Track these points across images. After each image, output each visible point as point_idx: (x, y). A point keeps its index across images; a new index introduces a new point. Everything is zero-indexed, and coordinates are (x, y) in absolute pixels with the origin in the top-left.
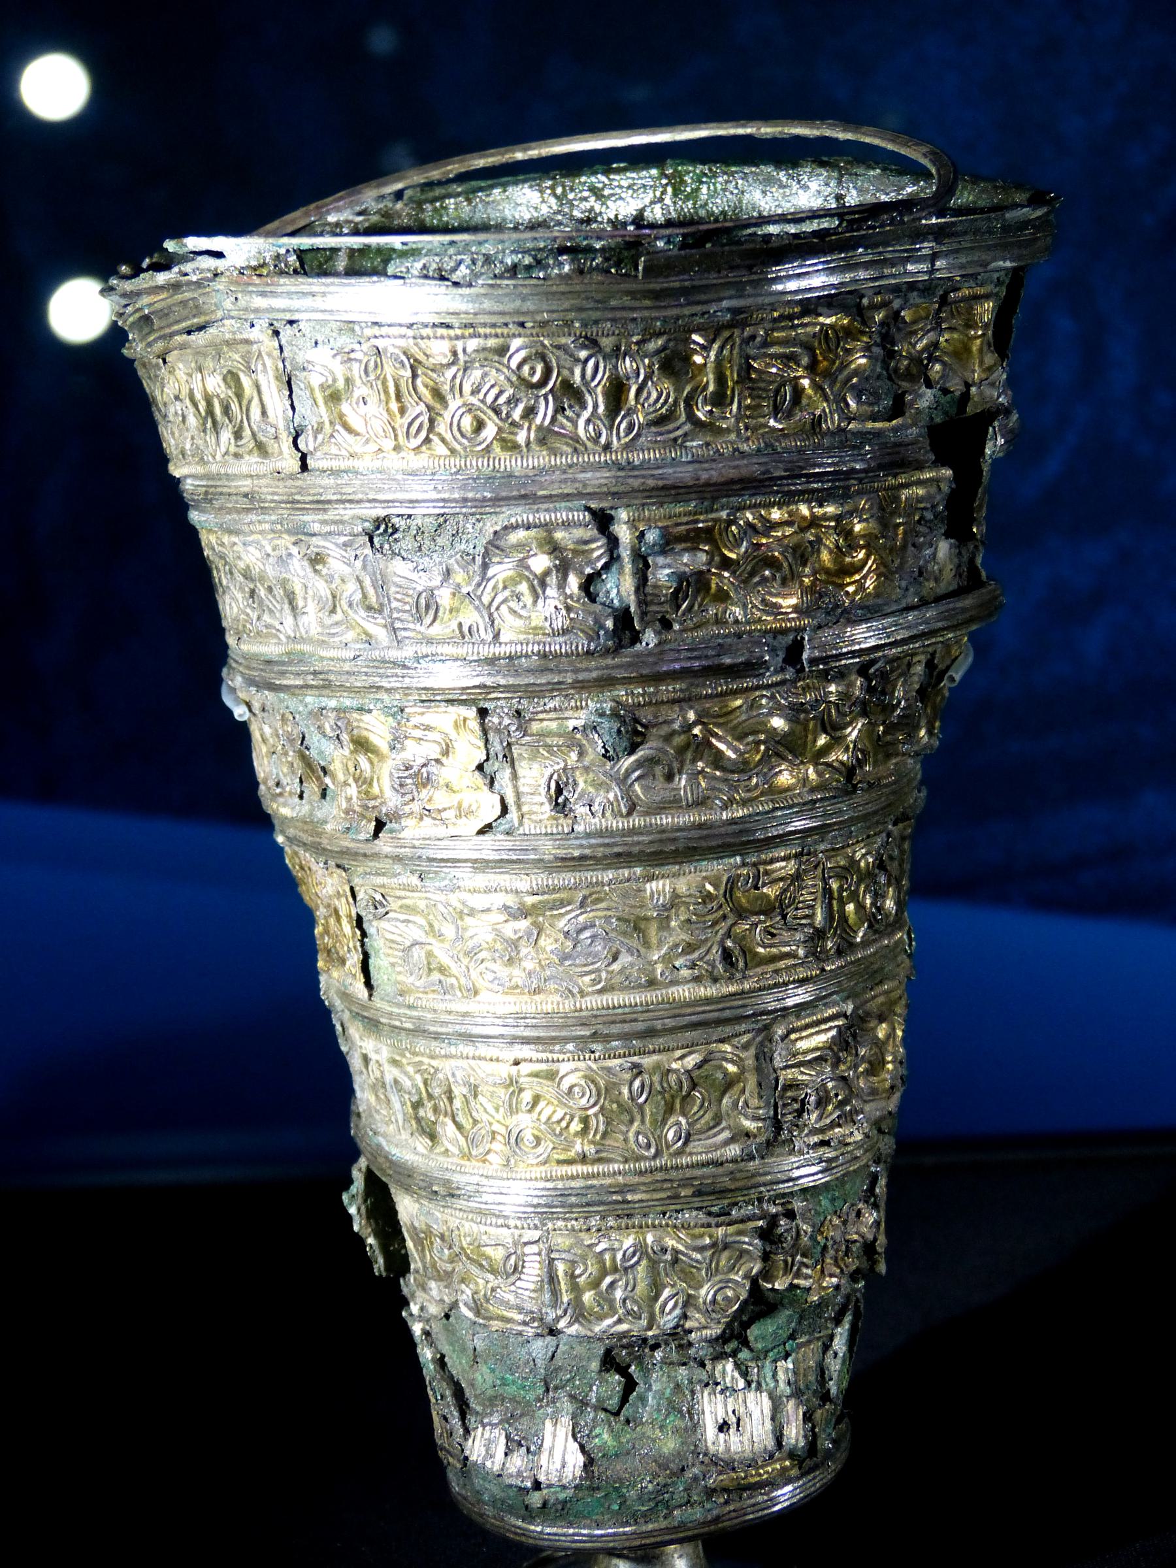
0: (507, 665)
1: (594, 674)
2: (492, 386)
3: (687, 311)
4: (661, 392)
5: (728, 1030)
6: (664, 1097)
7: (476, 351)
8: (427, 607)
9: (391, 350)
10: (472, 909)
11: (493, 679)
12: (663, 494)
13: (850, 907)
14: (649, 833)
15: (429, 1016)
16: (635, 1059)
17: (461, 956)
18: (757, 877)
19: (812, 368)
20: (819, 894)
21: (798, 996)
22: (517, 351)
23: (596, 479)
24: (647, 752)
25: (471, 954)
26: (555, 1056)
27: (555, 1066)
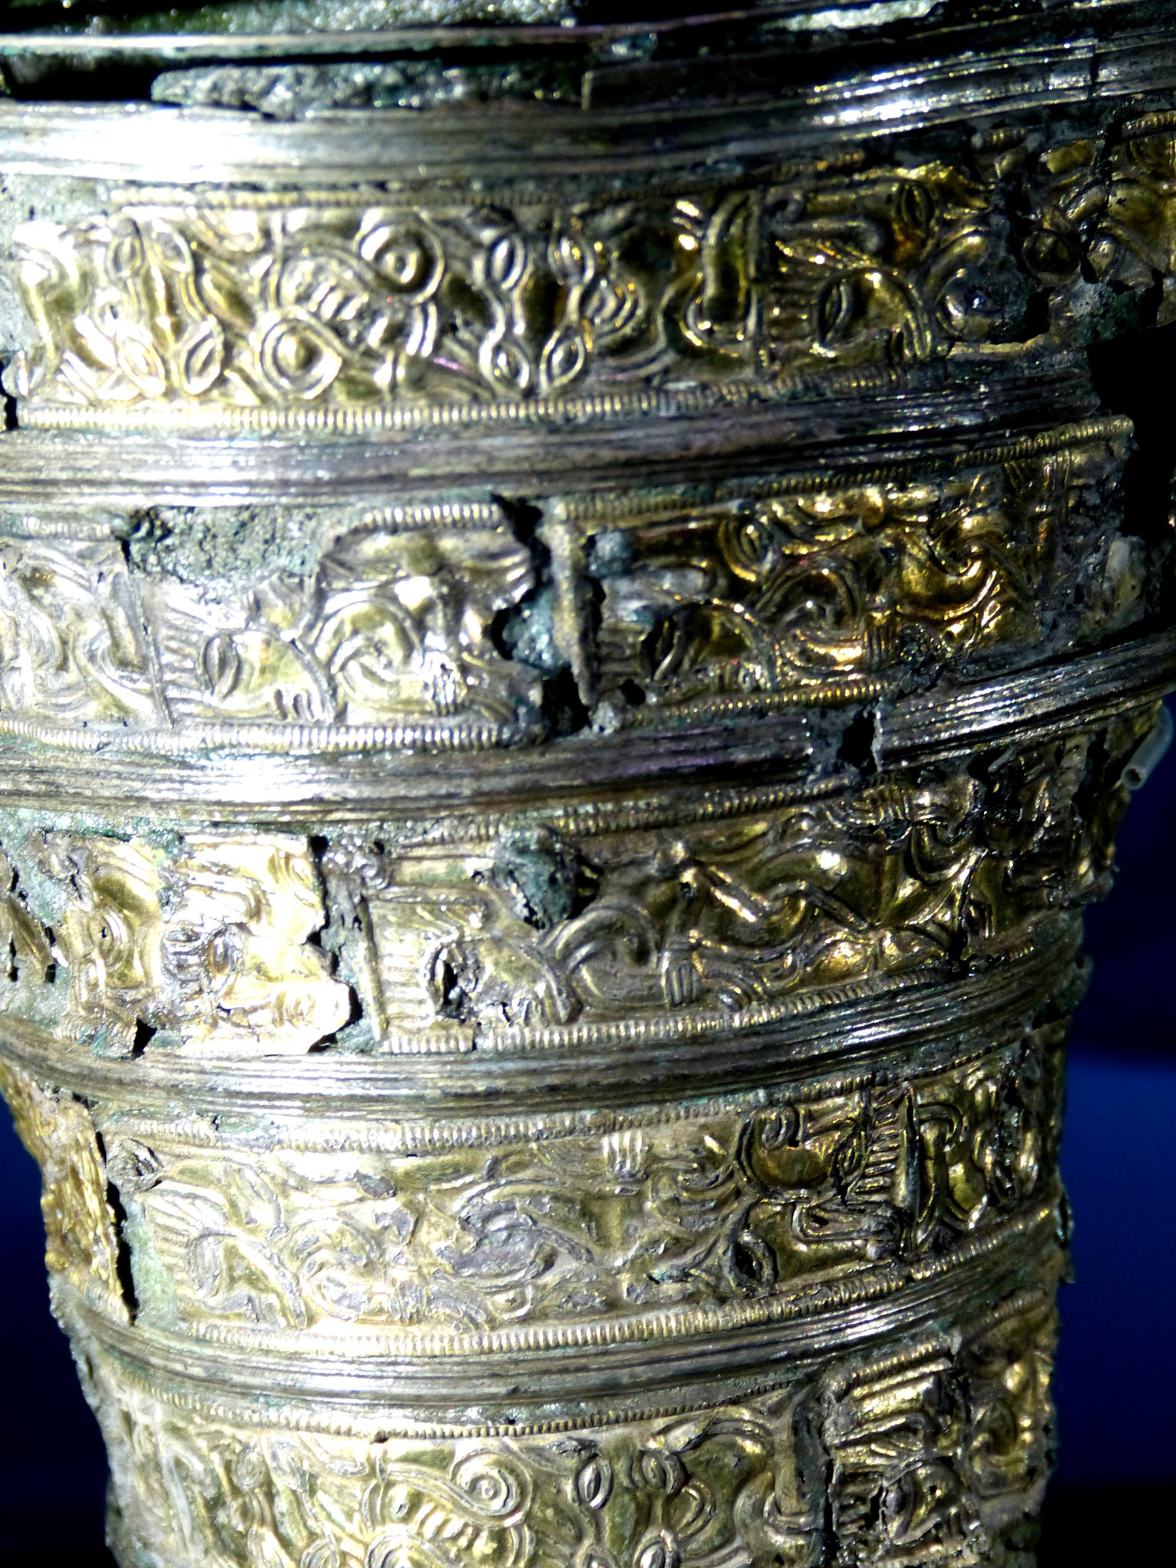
0: (360, 764)
1: (510, 781)
2: (332, 289)
3: (666, 162)
4: (621, 301)
5: (746, 1383)
6: (635, 1498)
7: (305, 230)
8: (221, 663)
9: (159, 227)
10: (303, 1179)
11: (335, 789)
12: (628, 472)
13: (958, 1171)
14: (606, 1052)
15: (233, 1357)
16: (585, 1433)
17: (285, 1257)
18: (794, 1125)
19: (886, 256)
20: (903, 1151)
21: (870, 1323)
22: (375, 229)
23: (510, 449)
24: (604, 914)
25: (302, 1253)
26: (447, 1429)
27: (447, 1445)
